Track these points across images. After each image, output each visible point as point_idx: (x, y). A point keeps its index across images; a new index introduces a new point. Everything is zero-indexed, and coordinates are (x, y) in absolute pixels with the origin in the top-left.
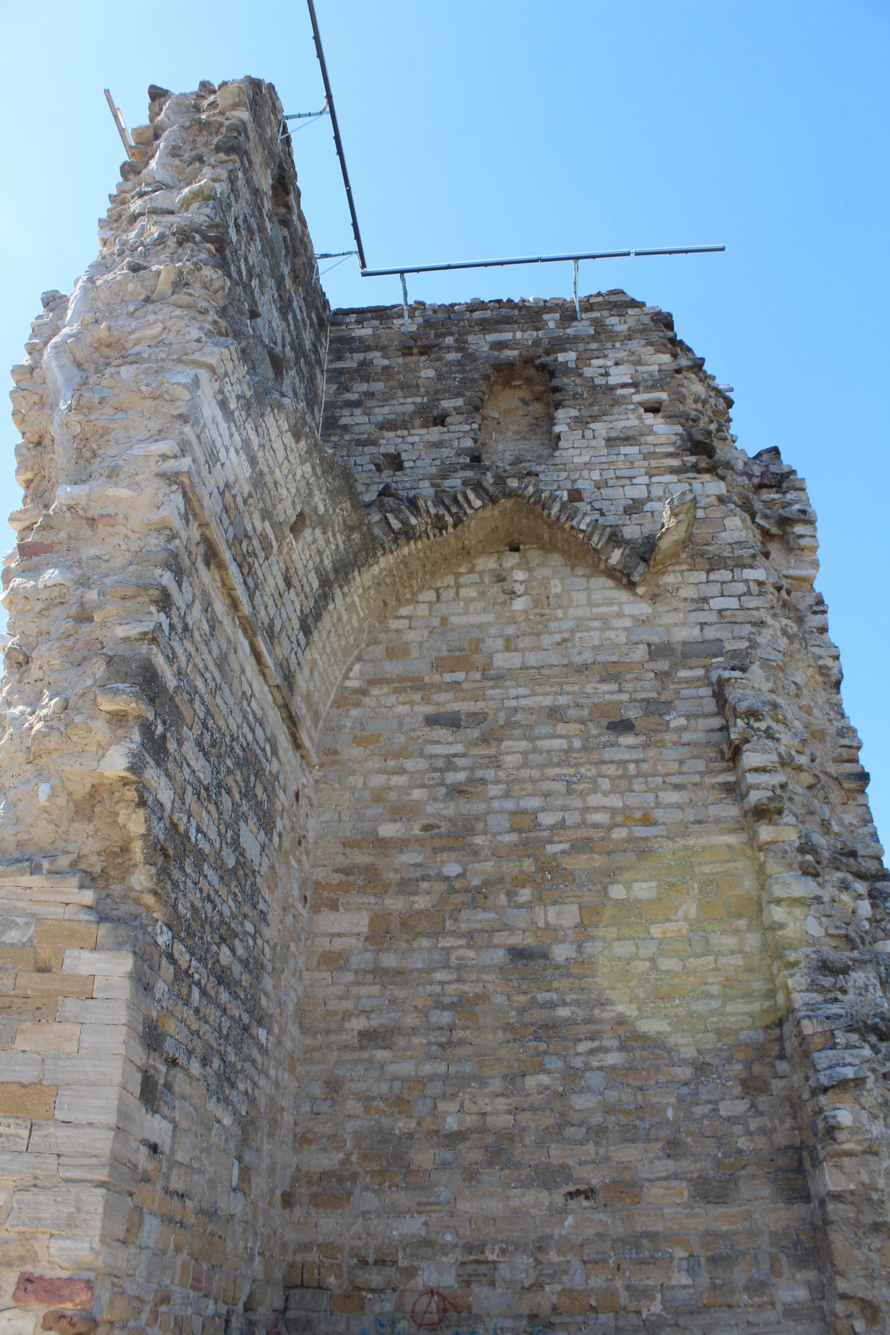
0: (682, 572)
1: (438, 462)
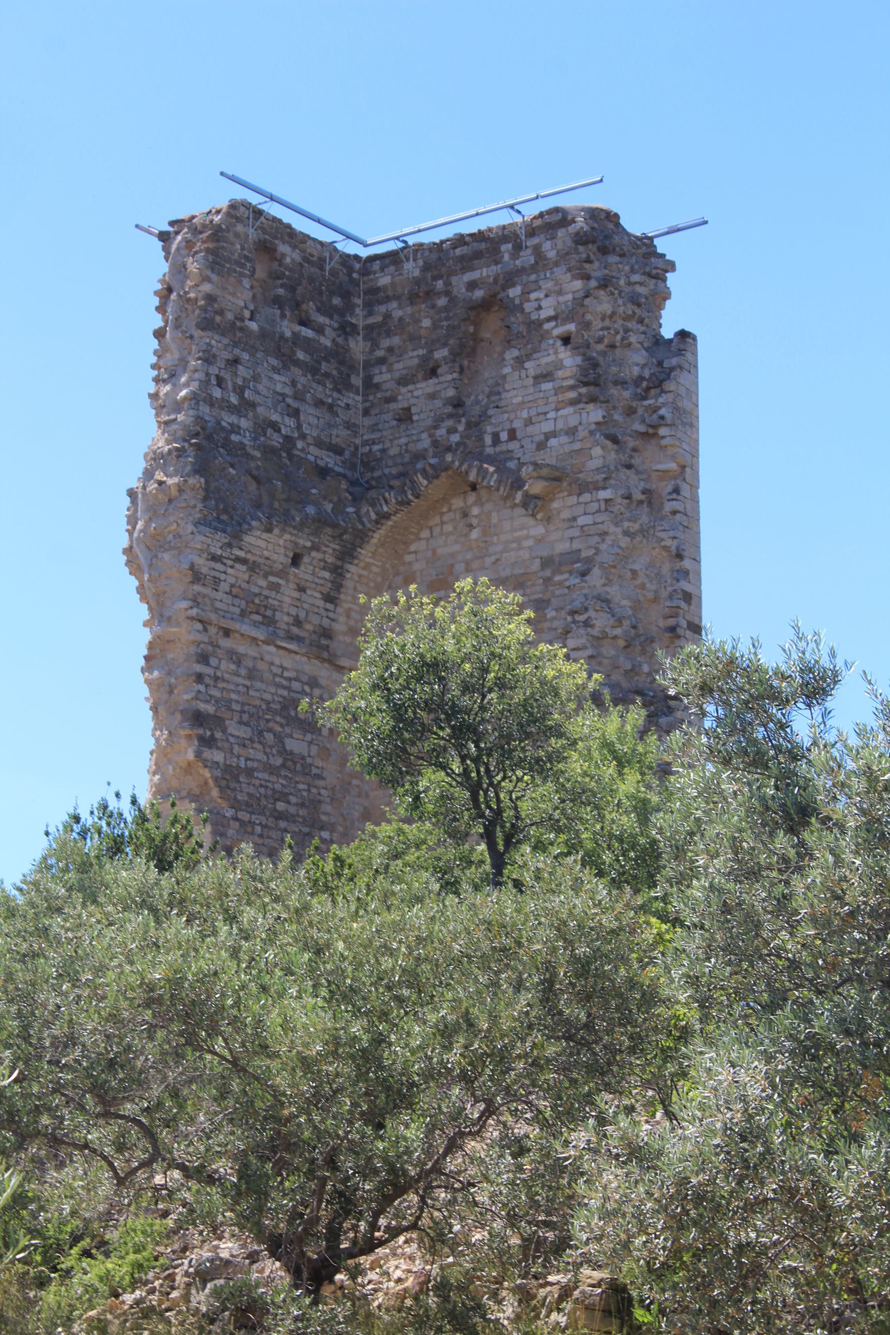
0: (563, 498)
1: (432, 414)
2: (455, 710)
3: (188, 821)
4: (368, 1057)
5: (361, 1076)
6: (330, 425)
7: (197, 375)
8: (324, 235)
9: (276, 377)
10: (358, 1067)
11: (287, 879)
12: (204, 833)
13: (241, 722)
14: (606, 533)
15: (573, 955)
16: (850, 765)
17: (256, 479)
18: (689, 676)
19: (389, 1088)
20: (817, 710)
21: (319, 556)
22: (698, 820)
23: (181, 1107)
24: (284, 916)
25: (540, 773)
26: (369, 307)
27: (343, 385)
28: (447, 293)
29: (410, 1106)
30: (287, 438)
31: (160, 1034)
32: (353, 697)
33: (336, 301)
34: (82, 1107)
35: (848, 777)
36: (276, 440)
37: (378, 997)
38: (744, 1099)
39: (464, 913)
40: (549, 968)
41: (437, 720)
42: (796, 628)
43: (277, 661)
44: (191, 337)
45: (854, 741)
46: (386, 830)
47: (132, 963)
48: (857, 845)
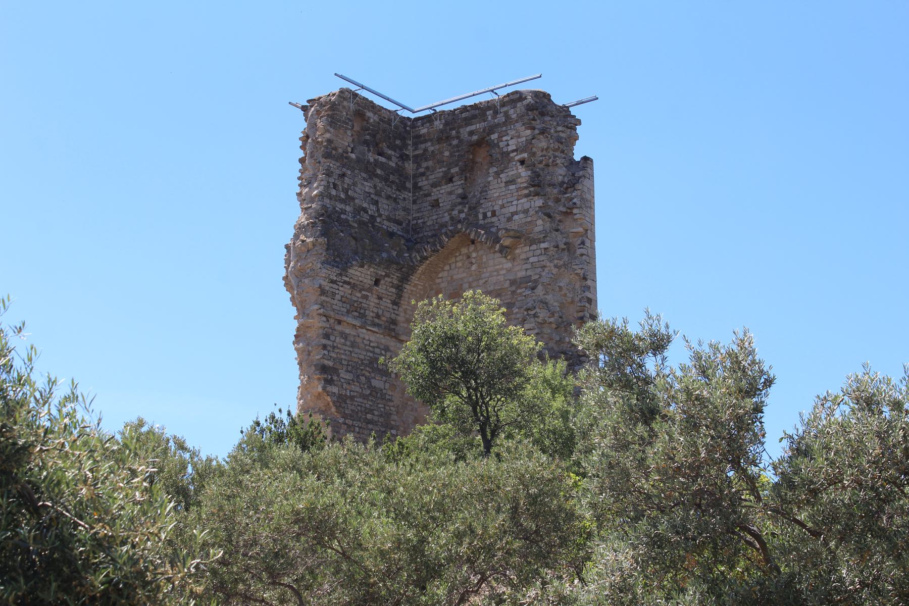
2: (464, 362)
3: (319, 425)
4: (417, 550)
5: (413, 560)
6: (395, 209)
7: (322, 183)
8: (391, 107)
9: (366, 183)
10: (411, 555)
11: (372, 455)
12: (327, 431)
13: (347, 371)
14: (545, 266)
15: (528, 493)
16: (677, 386)
17: (355, 239)
18: (589, 339)
19: (427, 567)
20: (659, 357)
21: (389, 280)
22: (595, 418)
23: (315, 579)
24: (370, 473)
25: (510, 396)
26: (416, 145)
27: (402, 187)
28: (458, 138)
29: (440, 576)
30: (371, 216)
31: (303, 539)
32: (408, 356)
33: (398, 142)
34: (261, 580)
35: (676, 393)
36: (365, 218)
37: (421, 517)
38: (621, 569)
39: (469, 471)
40: (515, 500)
41: (454, 368)
42: (647, 312)
43: (367, 338)
44: (319, 162)
45: (679, 373)
46: (427, 428)
47: (287, 500)
48: (681, 429)
